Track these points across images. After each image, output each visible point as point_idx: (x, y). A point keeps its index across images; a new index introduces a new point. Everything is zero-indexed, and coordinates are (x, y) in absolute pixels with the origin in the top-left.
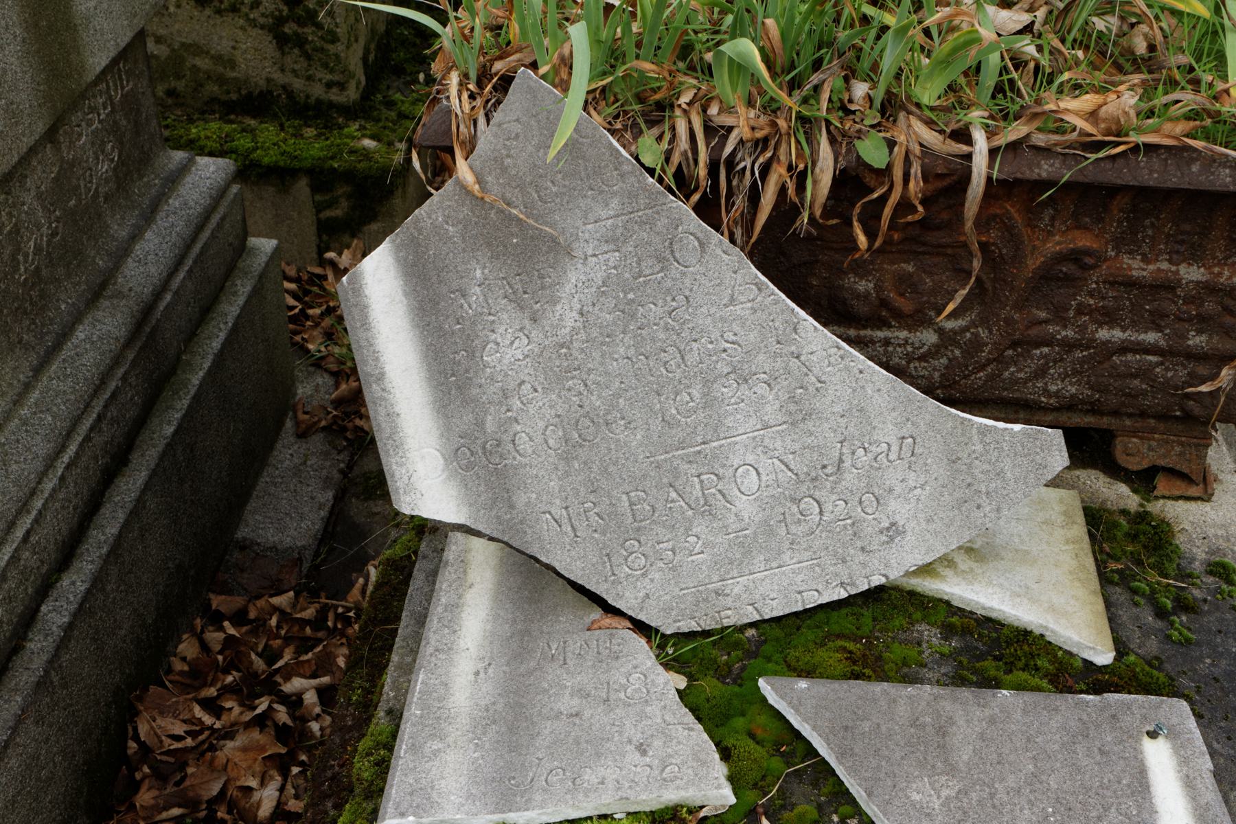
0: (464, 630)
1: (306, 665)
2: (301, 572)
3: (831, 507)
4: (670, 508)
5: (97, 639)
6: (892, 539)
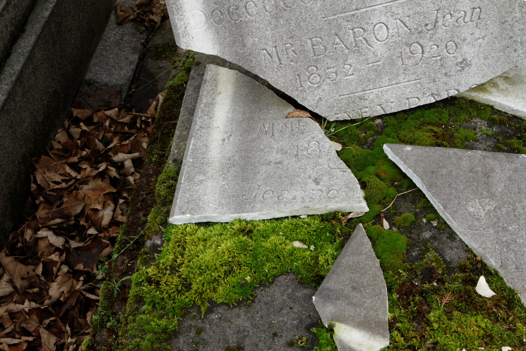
0: (216, 116)
1: (126, 147)
2: (121, 98)
3: (429, 49)
4: (336, 48)
5: (12, 127)
6: (463, 68)
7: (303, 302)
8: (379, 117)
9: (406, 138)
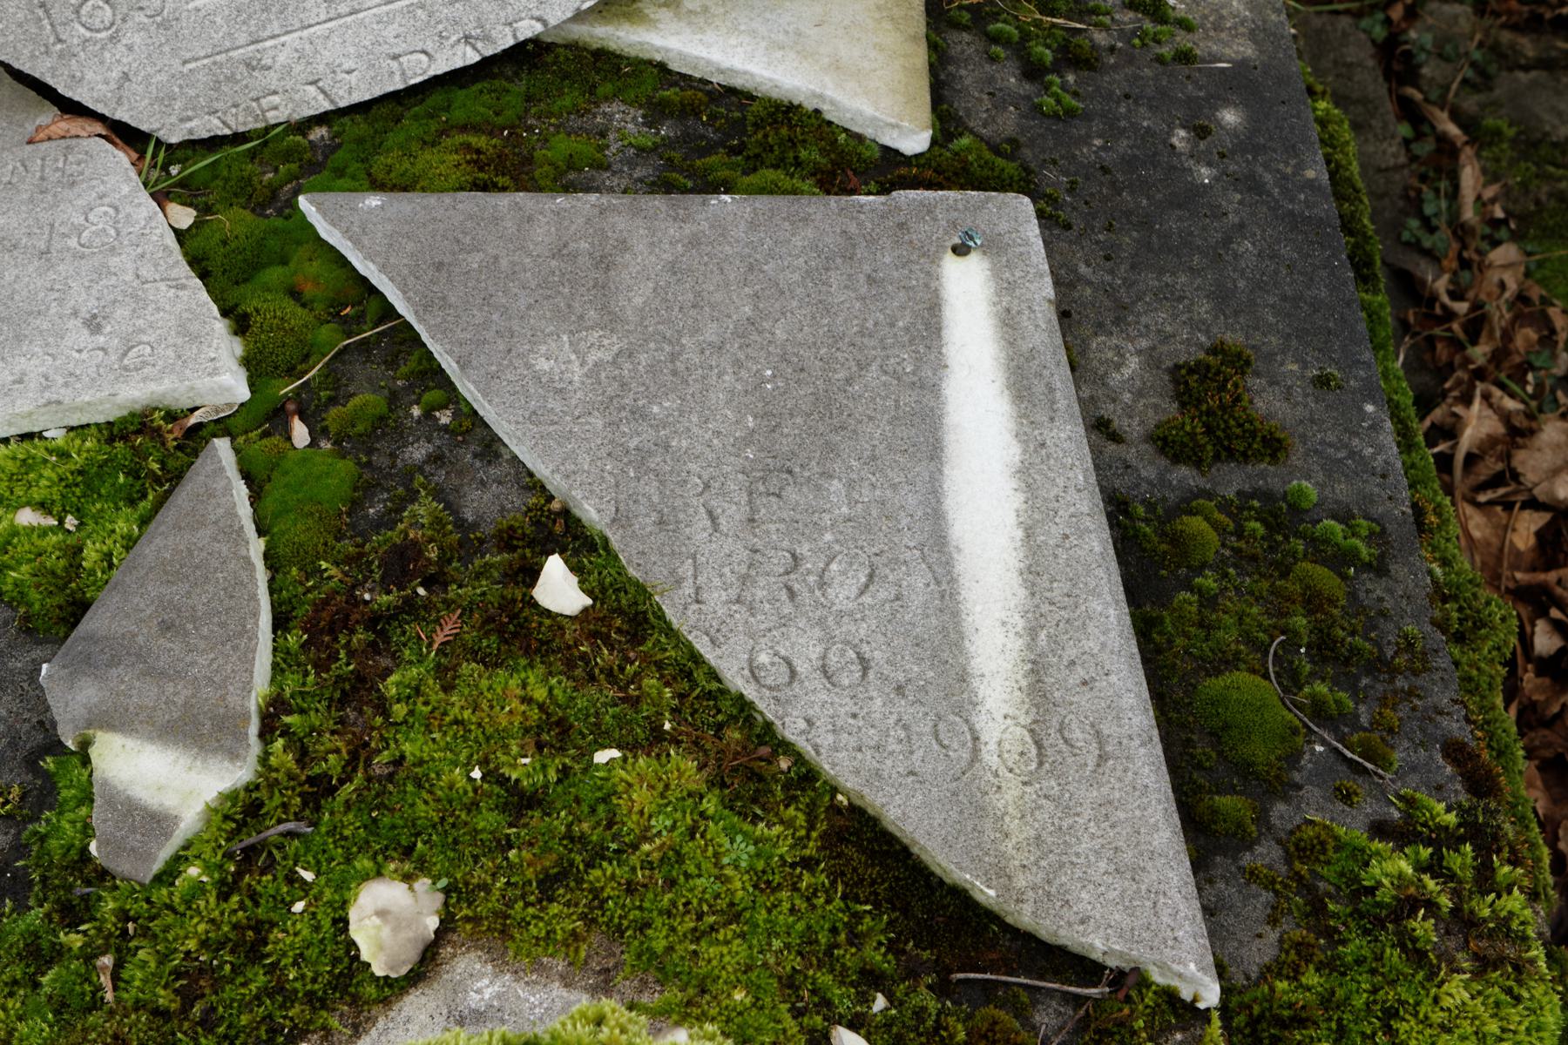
7: (25, 685)
8: (322, 119)
9: (393, 175)
